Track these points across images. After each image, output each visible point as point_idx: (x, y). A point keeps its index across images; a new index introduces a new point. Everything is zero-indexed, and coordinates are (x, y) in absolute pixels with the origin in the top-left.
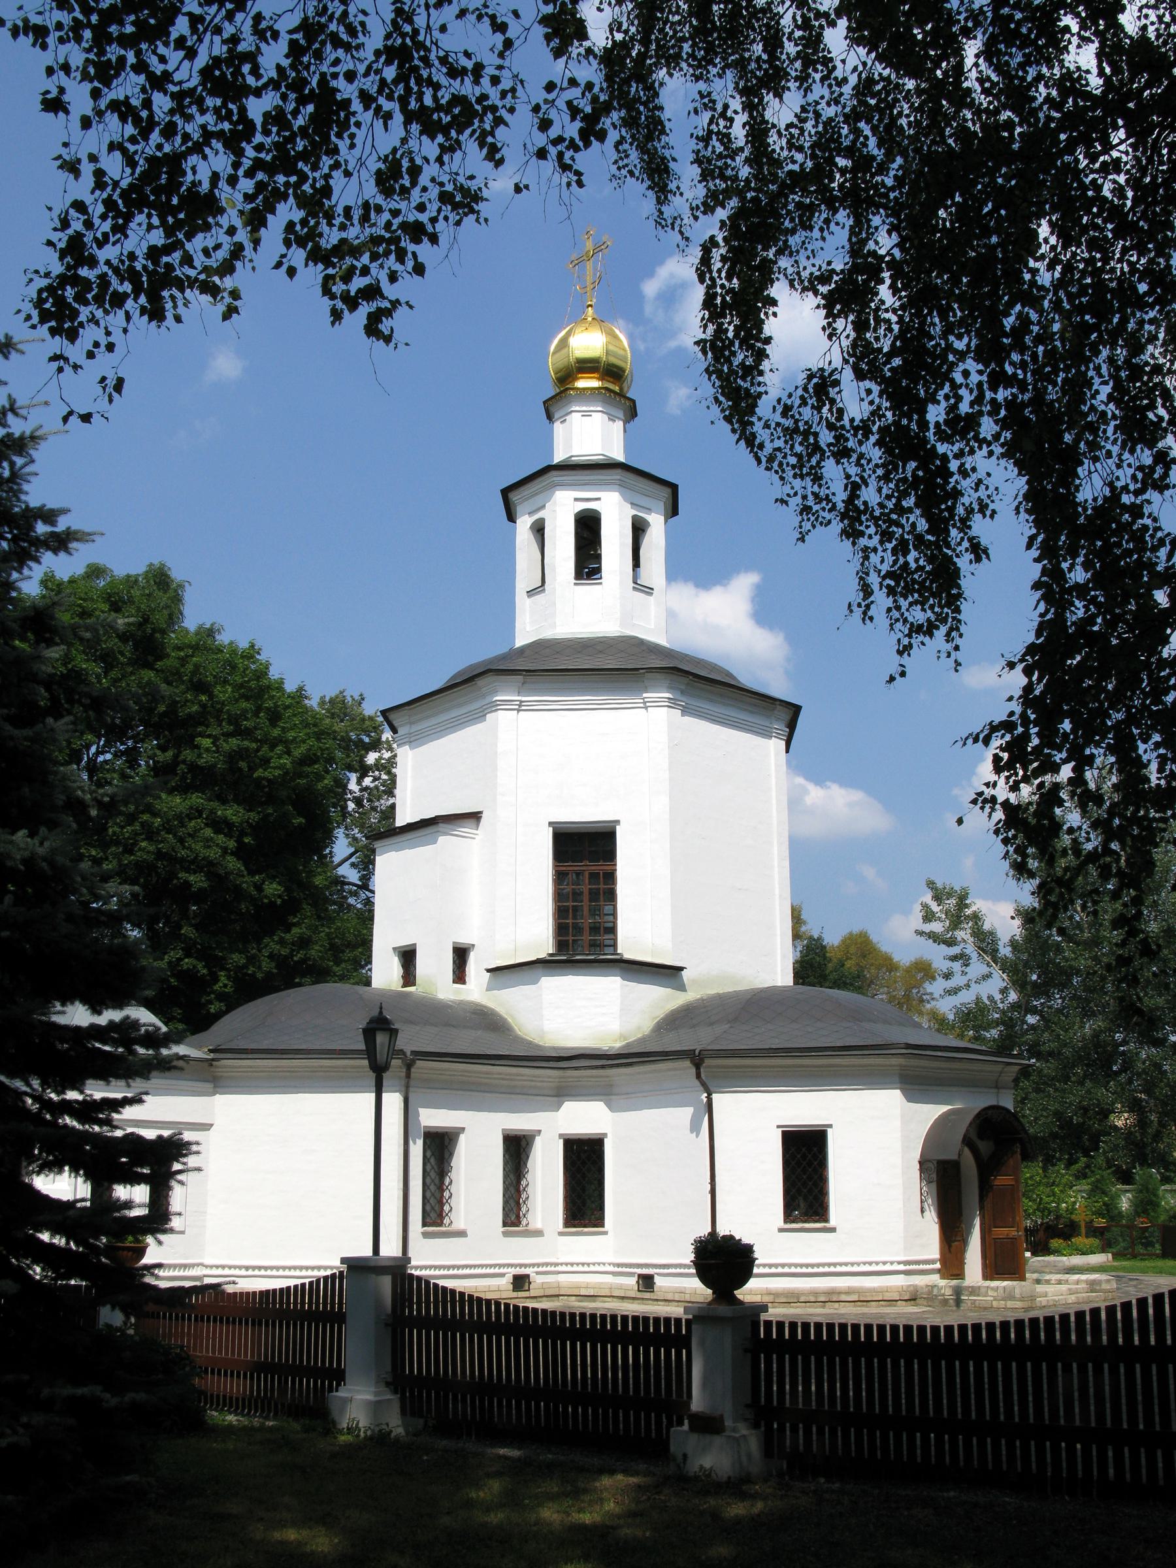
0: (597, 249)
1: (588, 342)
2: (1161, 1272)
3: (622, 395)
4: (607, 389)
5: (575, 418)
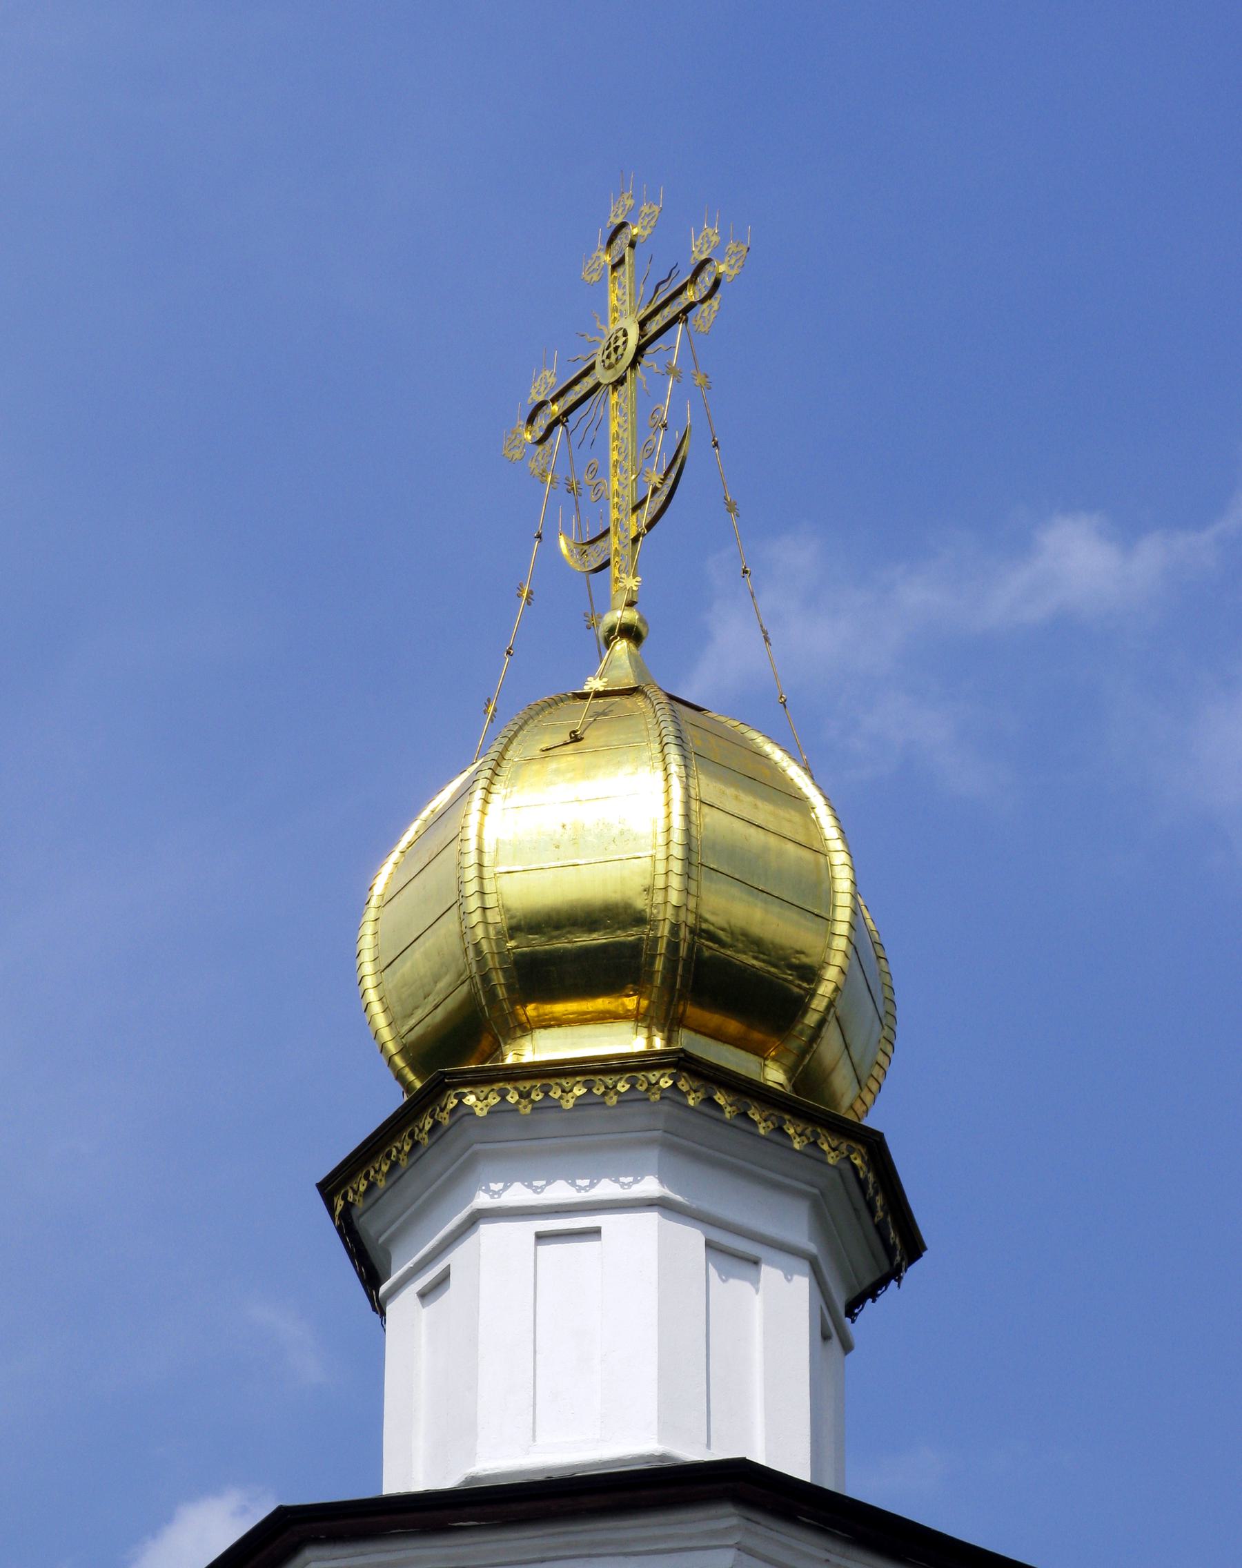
0: (663, 318)
1: (582, 821)
2: (718, 1518)
3: (807, 1104)
4: (682, 1063)
5: (496, 1261)
